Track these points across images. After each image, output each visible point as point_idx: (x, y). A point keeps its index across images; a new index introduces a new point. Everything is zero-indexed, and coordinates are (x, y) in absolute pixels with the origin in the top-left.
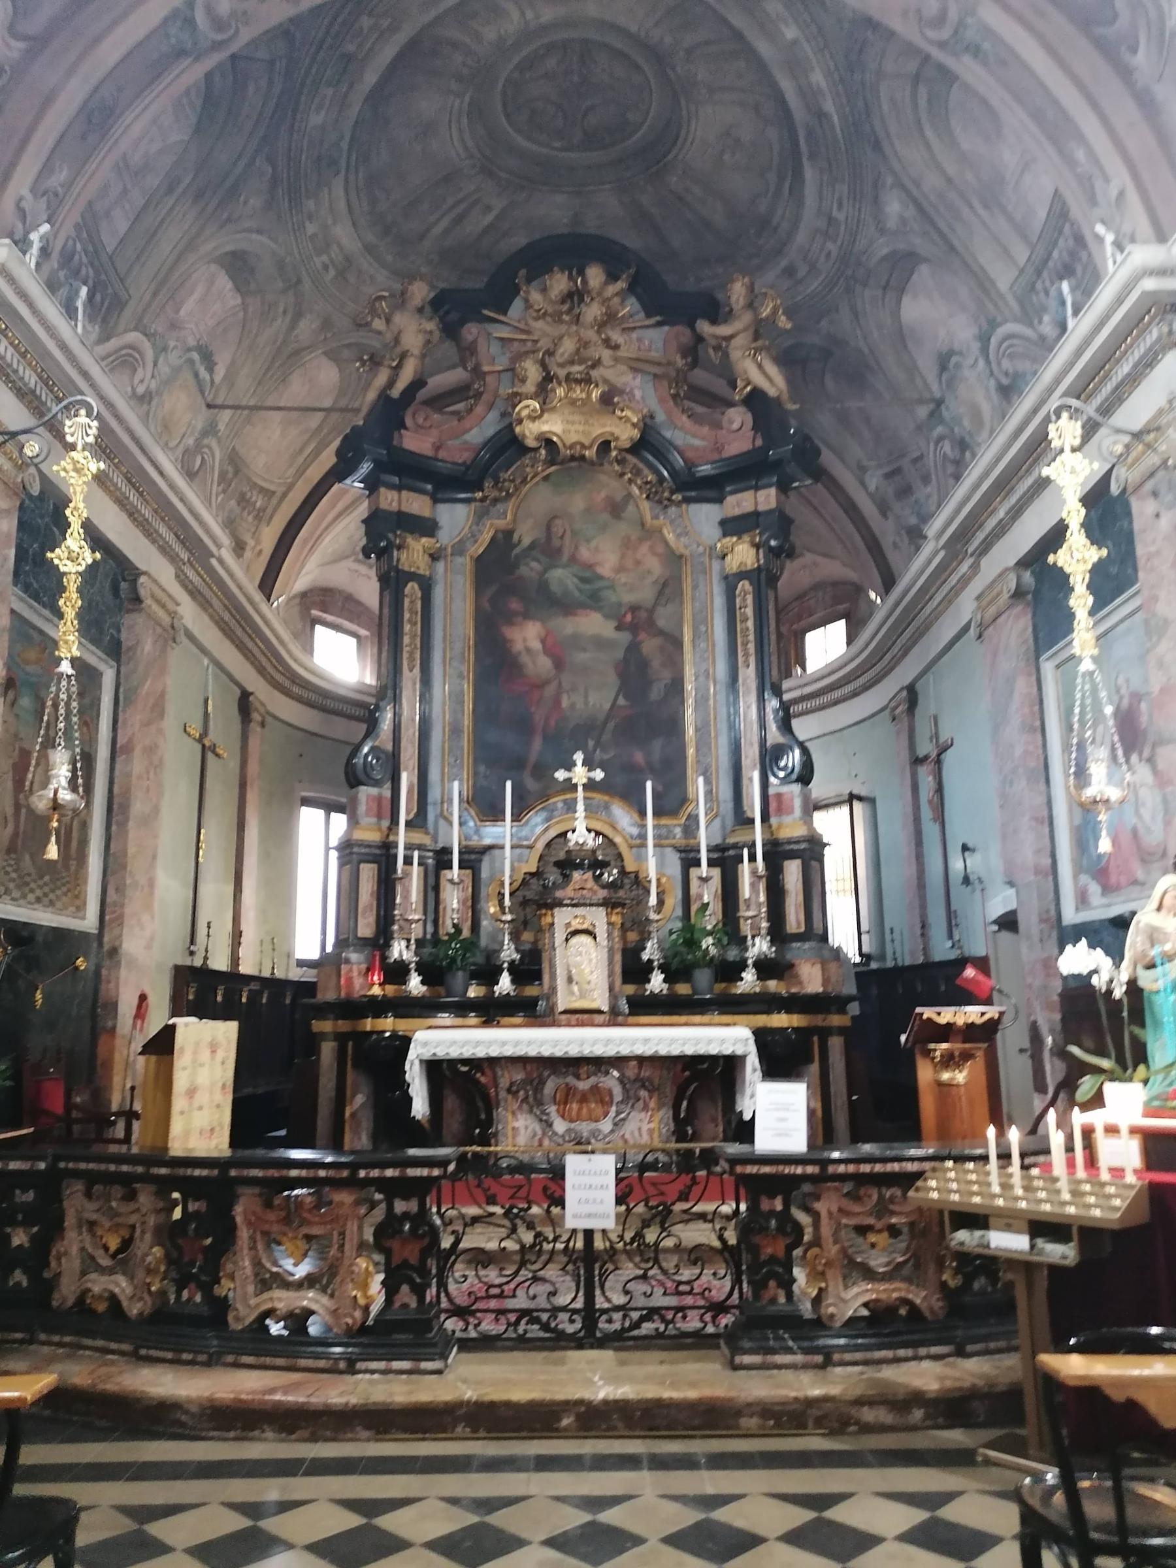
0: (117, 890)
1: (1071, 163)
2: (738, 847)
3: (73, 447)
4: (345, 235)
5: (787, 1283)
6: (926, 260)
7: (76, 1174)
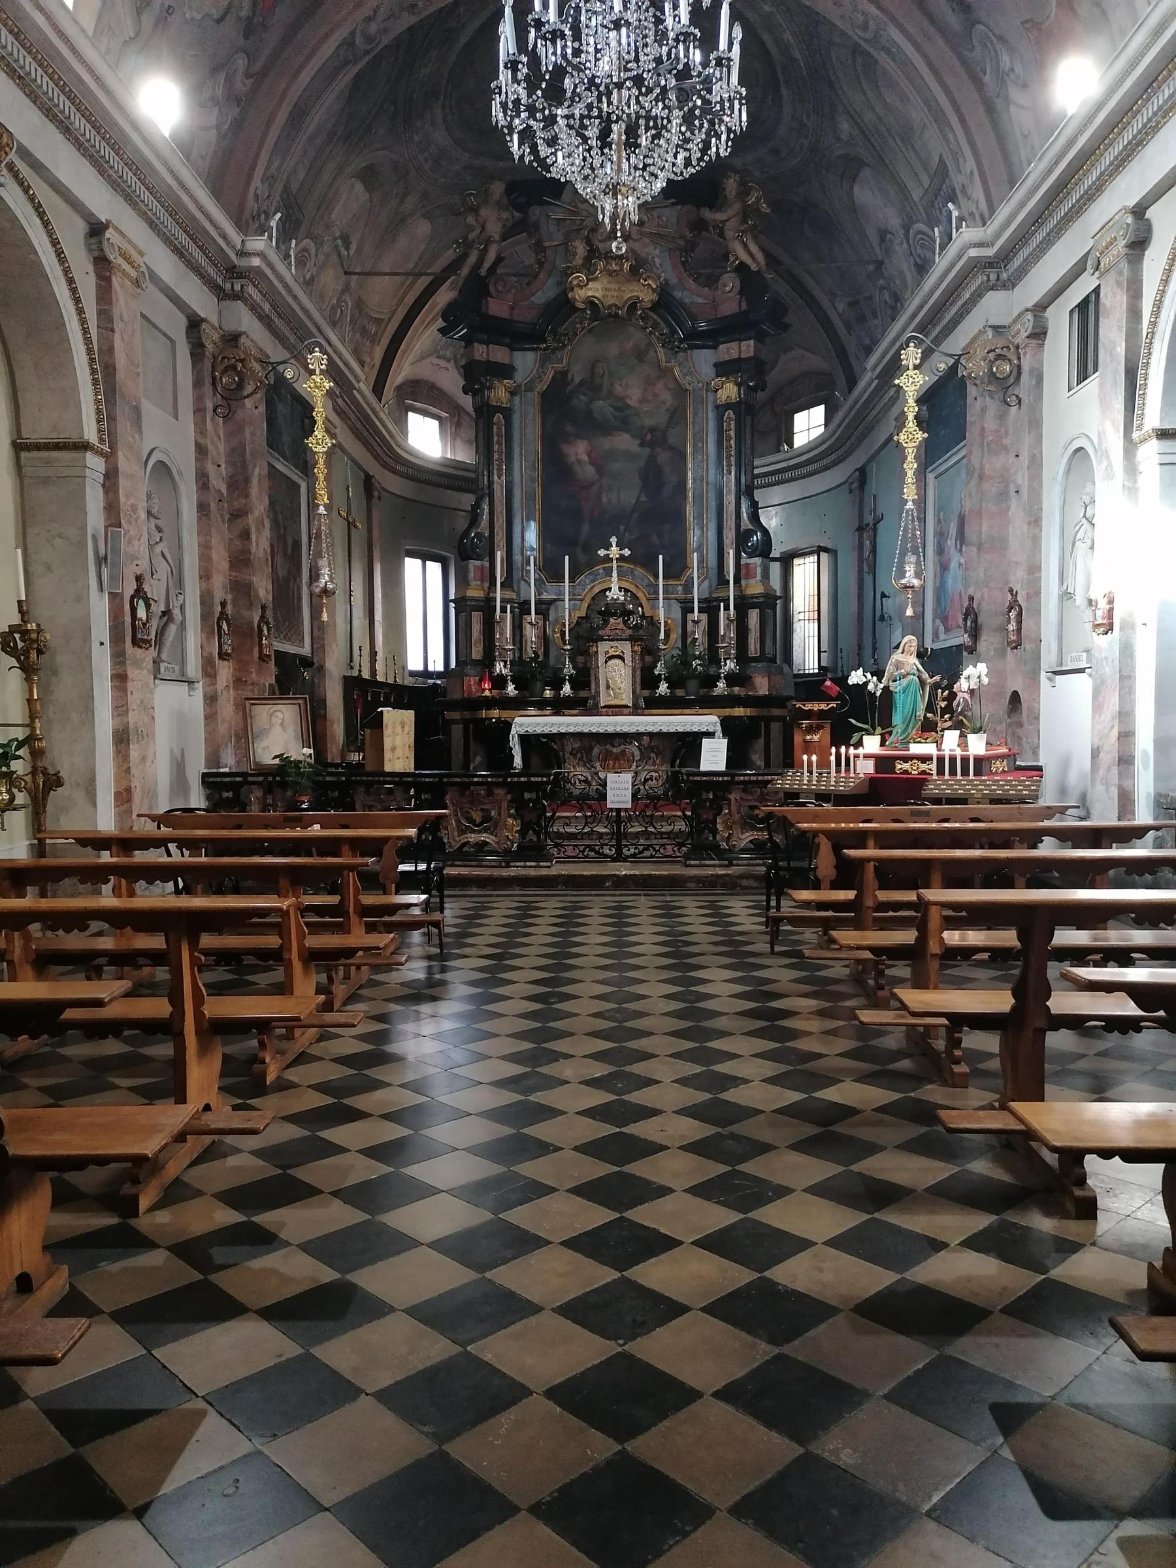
0: (319, 629)
1: (948, 141)
2: (718, 600)
3: (312, 372)
4: (440, 137)
5: (715, 832)
6: (868, 165)
7: (361, 783)
